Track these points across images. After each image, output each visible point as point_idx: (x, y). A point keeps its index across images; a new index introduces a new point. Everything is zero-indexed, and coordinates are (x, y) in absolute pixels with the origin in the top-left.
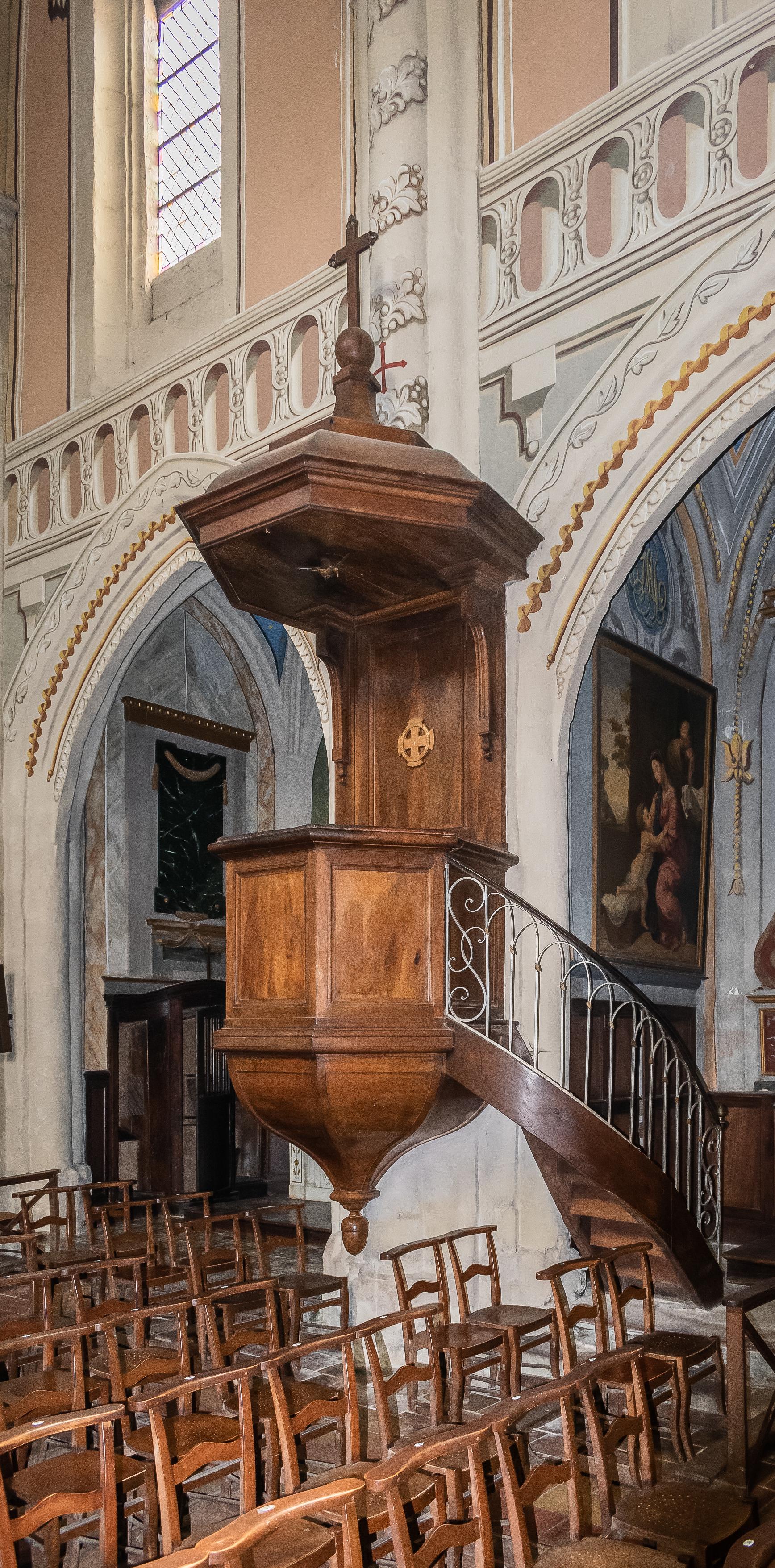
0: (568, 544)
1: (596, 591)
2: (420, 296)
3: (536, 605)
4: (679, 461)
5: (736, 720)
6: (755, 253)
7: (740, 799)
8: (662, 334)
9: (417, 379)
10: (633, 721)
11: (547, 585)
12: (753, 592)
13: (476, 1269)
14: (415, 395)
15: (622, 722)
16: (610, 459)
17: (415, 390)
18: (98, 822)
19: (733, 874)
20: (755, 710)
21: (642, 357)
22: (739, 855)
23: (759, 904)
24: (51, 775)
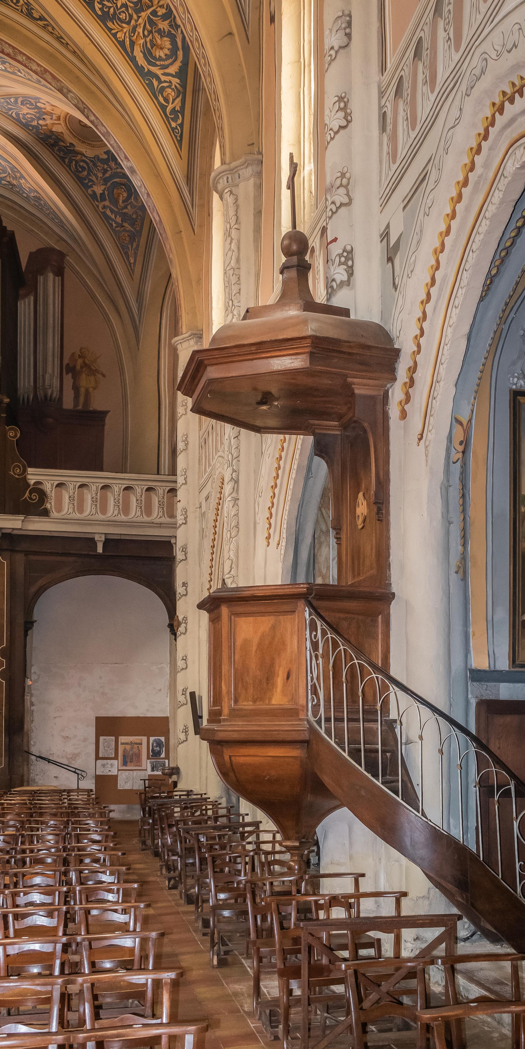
2: (346, 187)
3: (408, 398)
9: (345, 247)
14: (343, 259)
16: (429, 280)
17: (343, 256)
18: (324, 571)
24: (278, 544)
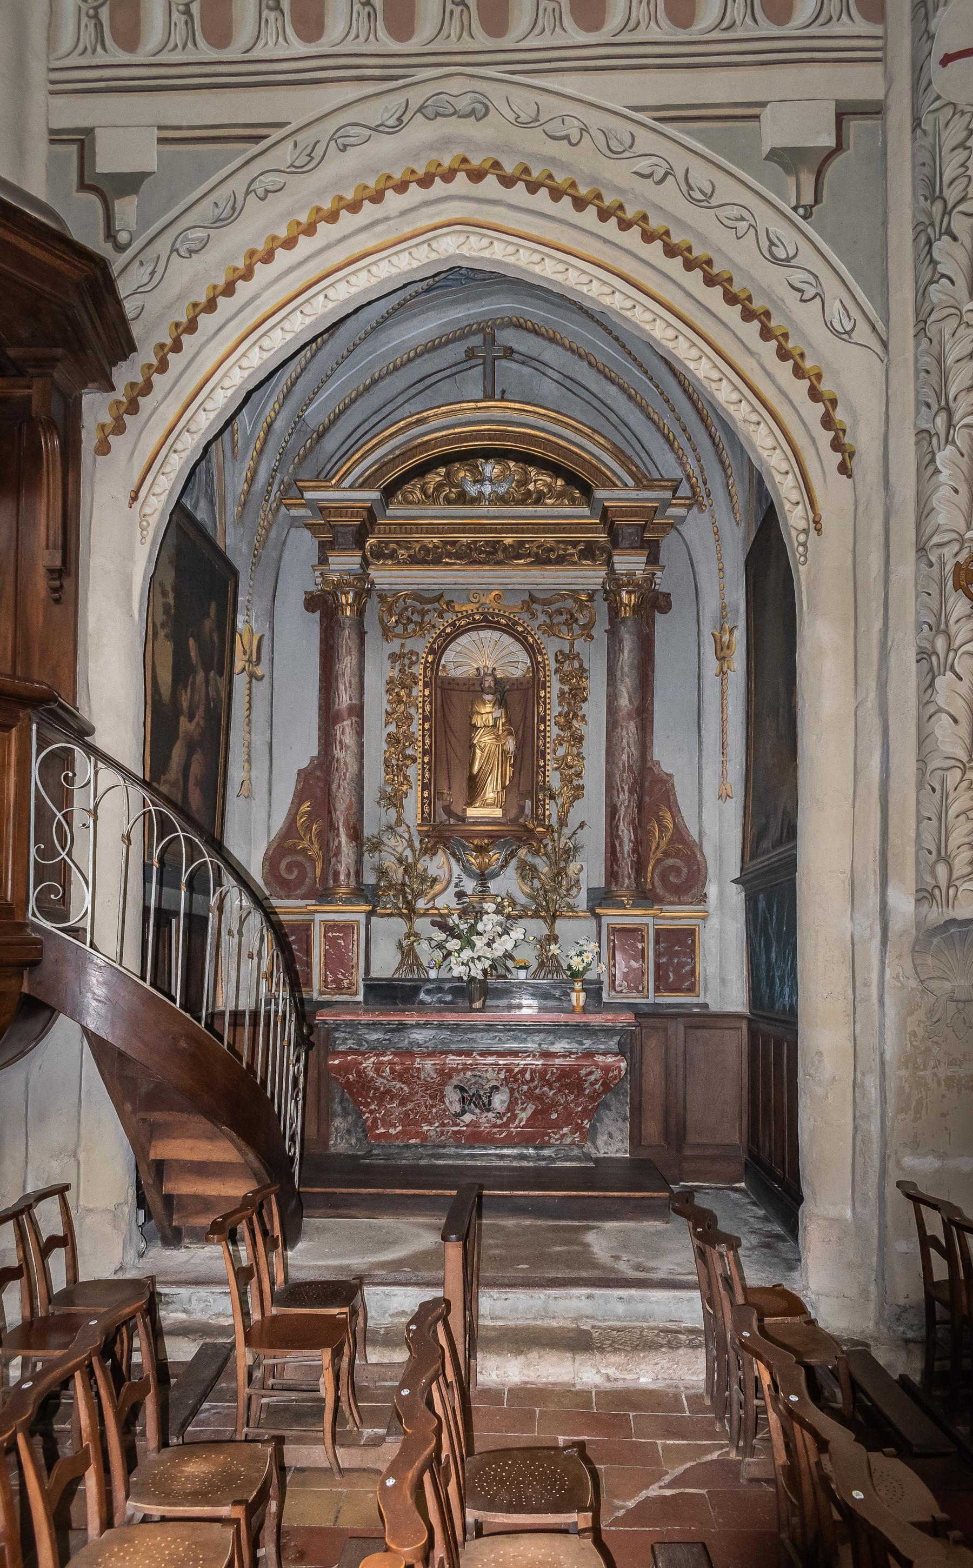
0: (163, 367)
1: (192, 429)
4: (298, 312)
5: (248, 610)
6: (399, 119)
7: (250, 695)
8: (292, 166)
10: (176, 589)
11: (133, 408)
12: (273, 477)
13: (55, 1242)
15: (169, 588)
16: (221, 282)
19: (243, 775)
20: (267, 602)
21: (270, 180)
22: (249, 754)
23: (267, 809)
